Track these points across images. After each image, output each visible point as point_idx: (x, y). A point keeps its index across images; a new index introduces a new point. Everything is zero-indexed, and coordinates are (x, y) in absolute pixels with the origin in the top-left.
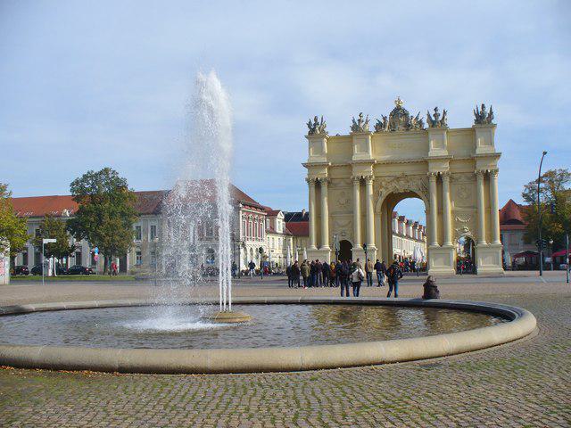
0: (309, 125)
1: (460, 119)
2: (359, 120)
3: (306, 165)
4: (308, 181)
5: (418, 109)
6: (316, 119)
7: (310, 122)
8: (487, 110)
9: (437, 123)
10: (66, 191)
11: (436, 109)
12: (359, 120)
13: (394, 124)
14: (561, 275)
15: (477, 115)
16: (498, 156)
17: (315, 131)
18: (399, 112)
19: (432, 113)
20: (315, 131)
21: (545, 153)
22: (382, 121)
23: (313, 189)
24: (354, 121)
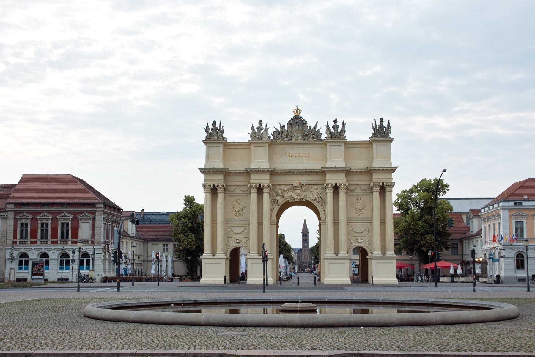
0: (207, 129)
1: (359, 131)
2: (258, 128)
3: (203, 171)
4: (204, 186)
5: (318, 119)
6: (214, 123)
7: (207, 127)
8: (385, 124)
9: (337, 134)
10: (184, 206)
11: (335, 121)
12: (258, 128)
13: (291, 132)
14: (470, 286)
15: (375, 129)
16: (394, 169)
17: (214, 135)
18: (297, 121)
19: (331, 124)
20: (214, 135)
21: (444, 171)
22: (279, 129)
23: (209, 195)
24: (253, 129)
